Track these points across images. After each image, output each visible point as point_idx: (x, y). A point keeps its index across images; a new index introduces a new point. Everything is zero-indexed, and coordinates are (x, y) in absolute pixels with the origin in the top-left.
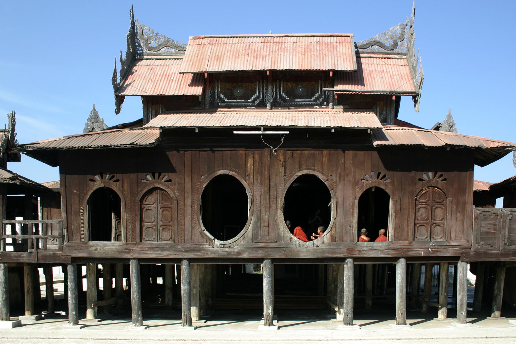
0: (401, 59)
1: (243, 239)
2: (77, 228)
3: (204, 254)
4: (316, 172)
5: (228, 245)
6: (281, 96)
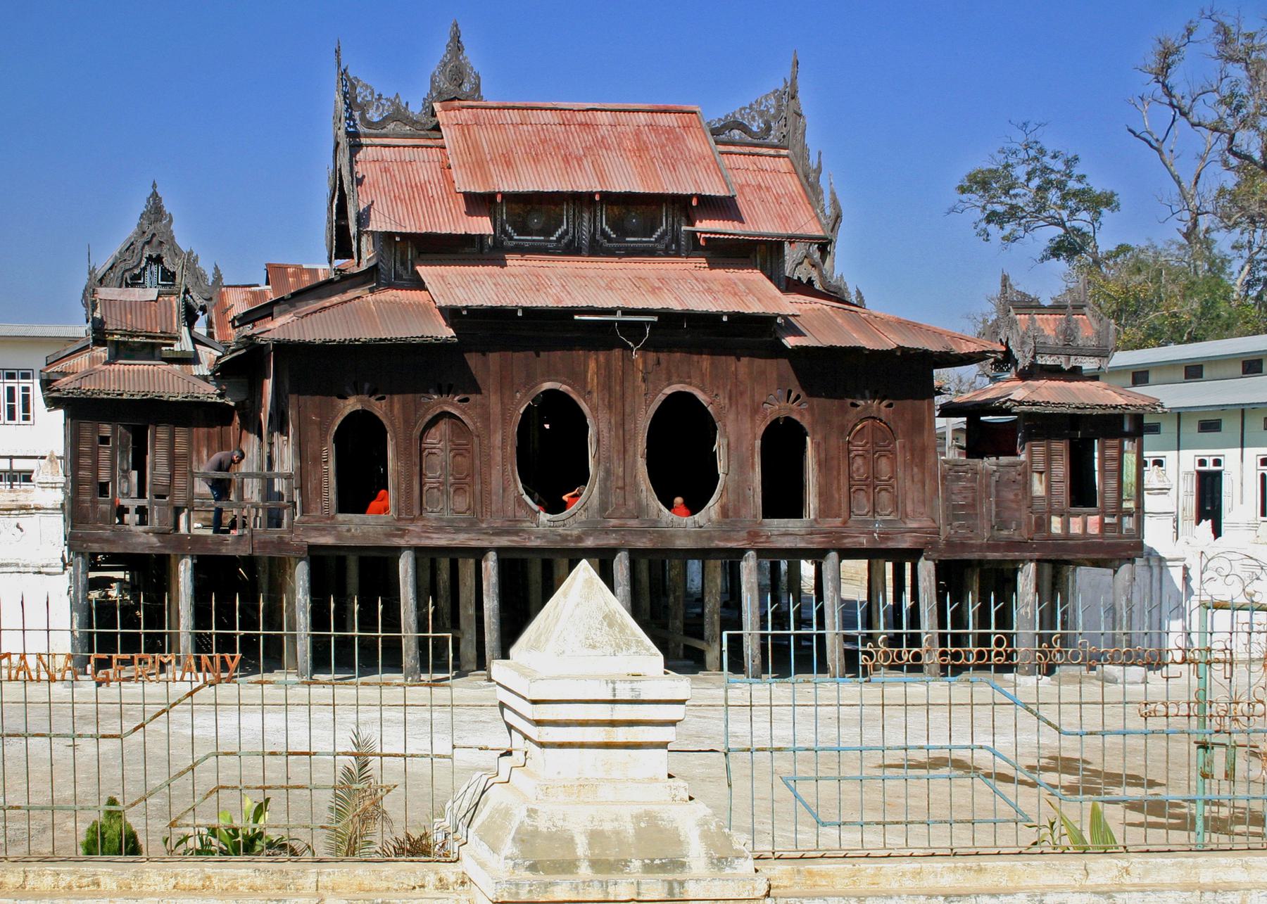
0: (779, 156)
1: (585, 511)
2: (316, 488)
3: (525, 539)
4: (694, 388)
5: (562, 523)
6: (603, 232)
